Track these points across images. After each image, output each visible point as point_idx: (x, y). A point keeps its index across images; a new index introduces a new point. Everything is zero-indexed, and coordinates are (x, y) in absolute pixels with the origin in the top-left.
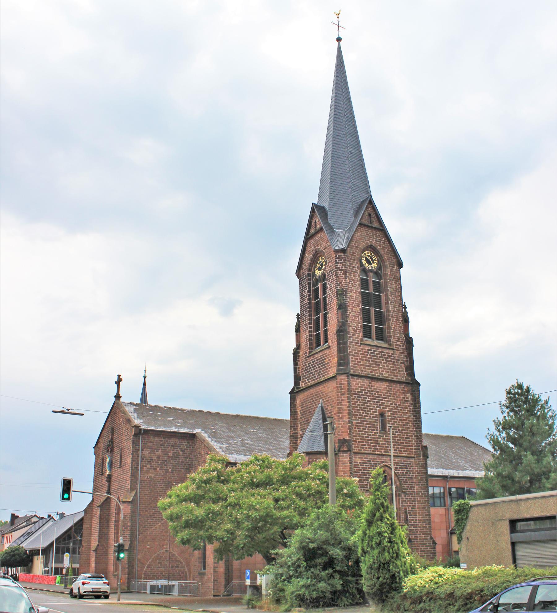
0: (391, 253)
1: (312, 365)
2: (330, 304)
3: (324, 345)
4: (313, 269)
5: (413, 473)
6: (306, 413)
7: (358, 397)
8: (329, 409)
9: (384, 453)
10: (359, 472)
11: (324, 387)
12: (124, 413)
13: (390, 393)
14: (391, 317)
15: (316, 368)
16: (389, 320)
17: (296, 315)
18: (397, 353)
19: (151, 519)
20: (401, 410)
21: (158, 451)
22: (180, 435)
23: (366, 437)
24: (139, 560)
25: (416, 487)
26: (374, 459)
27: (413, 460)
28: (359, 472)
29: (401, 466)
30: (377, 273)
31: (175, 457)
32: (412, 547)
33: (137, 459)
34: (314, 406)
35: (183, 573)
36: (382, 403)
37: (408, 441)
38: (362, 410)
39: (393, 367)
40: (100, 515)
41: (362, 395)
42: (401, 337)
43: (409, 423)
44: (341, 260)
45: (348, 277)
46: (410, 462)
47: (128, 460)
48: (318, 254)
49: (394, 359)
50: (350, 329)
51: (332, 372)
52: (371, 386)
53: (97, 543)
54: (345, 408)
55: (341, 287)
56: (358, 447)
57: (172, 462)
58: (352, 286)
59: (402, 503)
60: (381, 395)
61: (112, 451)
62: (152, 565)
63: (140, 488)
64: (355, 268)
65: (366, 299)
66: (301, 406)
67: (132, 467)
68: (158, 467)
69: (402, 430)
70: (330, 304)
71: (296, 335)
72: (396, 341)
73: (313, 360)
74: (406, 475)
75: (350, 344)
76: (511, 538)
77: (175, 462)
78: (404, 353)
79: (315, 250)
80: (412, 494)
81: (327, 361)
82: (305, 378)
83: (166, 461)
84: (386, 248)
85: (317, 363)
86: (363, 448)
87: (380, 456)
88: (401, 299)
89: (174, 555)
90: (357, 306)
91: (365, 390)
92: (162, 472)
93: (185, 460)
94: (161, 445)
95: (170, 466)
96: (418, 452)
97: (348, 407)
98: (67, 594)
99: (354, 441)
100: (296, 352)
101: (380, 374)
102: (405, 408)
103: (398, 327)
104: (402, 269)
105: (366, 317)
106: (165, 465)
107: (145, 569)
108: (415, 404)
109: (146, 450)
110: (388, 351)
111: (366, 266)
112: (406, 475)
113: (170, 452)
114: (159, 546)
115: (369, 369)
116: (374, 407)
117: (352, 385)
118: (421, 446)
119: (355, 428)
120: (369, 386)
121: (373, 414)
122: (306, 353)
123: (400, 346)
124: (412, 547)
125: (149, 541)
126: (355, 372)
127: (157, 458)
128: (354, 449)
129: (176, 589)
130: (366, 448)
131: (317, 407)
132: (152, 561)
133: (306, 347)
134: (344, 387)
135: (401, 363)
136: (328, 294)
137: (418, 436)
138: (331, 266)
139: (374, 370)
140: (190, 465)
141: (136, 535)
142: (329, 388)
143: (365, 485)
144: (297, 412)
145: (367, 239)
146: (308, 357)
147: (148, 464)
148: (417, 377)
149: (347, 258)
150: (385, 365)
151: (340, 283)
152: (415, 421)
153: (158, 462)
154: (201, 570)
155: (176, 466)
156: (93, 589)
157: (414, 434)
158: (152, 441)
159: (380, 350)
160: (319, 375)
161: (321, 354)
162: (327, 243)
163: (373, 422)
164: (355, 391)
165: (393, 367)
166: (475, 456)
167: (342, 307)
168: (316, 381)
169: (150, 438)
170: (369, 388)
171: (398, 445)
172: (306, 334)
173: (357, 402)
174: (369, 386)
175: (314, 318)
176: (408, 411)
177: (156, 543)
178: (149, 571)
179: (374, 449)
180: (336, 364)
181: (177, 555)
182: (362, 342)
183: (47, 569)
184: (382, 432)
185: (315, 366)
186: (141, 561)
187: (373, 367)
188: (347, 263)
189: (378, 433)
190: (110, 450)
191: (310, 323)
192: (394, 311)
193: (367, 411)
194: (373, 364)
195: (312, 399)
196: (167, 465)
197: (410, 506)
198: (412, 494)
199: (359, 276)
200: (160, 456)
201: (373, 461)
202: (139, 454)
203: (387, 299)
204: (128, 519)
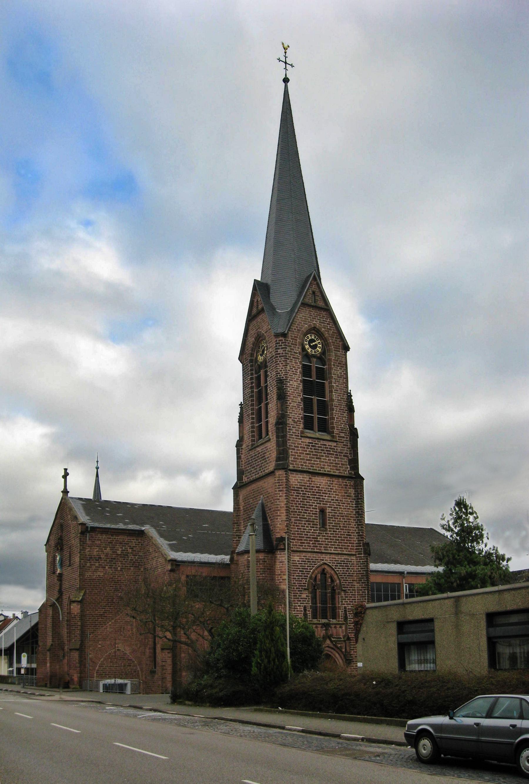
0: (337, 336)
1: (254, 459)
2: (271, 394)
3: (266, 437)
4: (255, 354)
5: (353, 571)
6: (249, 510)
7: (296, 493)
8: (269, 505)
9: (323, 551)
10: (297, 571)
11: (265, 482)
12: (71, 509)
13: (331, 489)
14: (335, 406)
15: (258, 462)
16: (333, 410)
19: (101, 619)
20: (343, 506)
21: (106, 549)
22: (127, 532)
23: (305, 535)
24: (91, 659)
25: (357, 585)
26: (313, 557)
27: (354, 558)
28: (297, 571)
29: (341, 564)
30: (321, 359)
31: (123, 555)
32: (351, 645)
34: (255, 502)
35: (136, 672)
36: (322, 499)
37: (350, 538)
38: (301, 507)
39: (335, 461)
41: (302, 491)
42: (345, 428)
43: (351, 520)
44: (282, 346)
45: (289, 364)
46: (351, 559)
47: (77, 559)
48: (260, 337)
49: (337, 452)
50: (290, 421)
51: (271, 467)
52: (312, 481)
55: (281, 375)
56: (296, 545)
58: (293, 374)
59: (342, 602)
60: (322, 490)
61: (62, 549)
64: (297, 353)
66: (244, 502)
67: (80, 566)
68: (107, 565)
69: (343, 527)
70: (271, 394)
71: (239, 425)
72: (339, 432)
73: (255, 453)
74: (346, 573)
75: (289, 437)
76: (488, 632)
77: (124, 559)
78: (347, 445)
79: (257, 333)
80: (353, 592)
81: (267, 455)
82: (248, 473)
83: (115, 559)
84: (331, 330)
85: (259, 456)
86: (302, 546)
87: (320, 554)
88: (347, 387)
89: (126, 654)
90: (298, 395)
91: (305, 486)
92: (111, 570)
94: (109, 543)
95: (119, 564)
96: (359, 549)
97: (286, 504)
99: (293, 539)
100: (239, 445)
101: (321, 468)
102: (347, 504)
103: (343, 417)
104: (348, 353)
105: (307, 405)
106: (113, 563)
108: (358, 499)
110: (330, 443)
111: (309, 351)
112: (346, 573)
113: (118, 550)
115: (309, 463)
116: (314, 503)
117: (291, 481)
118: (363, 543)
119: (294, 526)
120: (309, 481)
121: (313, 511)
122: (249, 446)
123: (344, 437)
124: (351, 645)
126: (295, 467)
128: (292, 548)
129: (129, 687)
130: (305, 546)
131: (258, 503)
132: (104, 660)
133: (248, 439)
135: (344, 456)
136: (268, 382)
137: (359, 533)
138: (271, 352)
139: (314, 464)
141: (87, 634)
142: (268, 483)
143: (304, 583)
144: (240, 508)
145: (311, 320)
146: (250, 450)
147: (96, 563)
148: (362, 472)
149: (288, 343)
150: (327, 458)
152: (357, 517)
153: (107, 561)
157: (356, 530)
158: (100, 539)
159: (322, 442)
160: (260, 470)
161: (262, 447)
162: (268, 326)
163: (313, 519)
164: (294, 487)
165: (335, 461)
167: (282, 396)
169: (97, 535)
170: (310, 484)
171: (339, 543)
172: (248, 425)
173: (296, 498)
174: (309, 481)
175: (257, 408)
176: (350, 506)
177: (107, 642)
179: (313, 546)
180: (275, 459)
182: (303, 435)
183: (11, 669)
184: (322, 529)
185: (257, 460)
187: (314, 461)
190: (59, 548)
192: (338, 400)
193: (307, 508)
194: (314, 458)
195: (254, 495)
197: (350, 604)
198: (353, 592)
199: (300, 363)
200: (108, 554)
201: (311, 559)
203: (331, 387)
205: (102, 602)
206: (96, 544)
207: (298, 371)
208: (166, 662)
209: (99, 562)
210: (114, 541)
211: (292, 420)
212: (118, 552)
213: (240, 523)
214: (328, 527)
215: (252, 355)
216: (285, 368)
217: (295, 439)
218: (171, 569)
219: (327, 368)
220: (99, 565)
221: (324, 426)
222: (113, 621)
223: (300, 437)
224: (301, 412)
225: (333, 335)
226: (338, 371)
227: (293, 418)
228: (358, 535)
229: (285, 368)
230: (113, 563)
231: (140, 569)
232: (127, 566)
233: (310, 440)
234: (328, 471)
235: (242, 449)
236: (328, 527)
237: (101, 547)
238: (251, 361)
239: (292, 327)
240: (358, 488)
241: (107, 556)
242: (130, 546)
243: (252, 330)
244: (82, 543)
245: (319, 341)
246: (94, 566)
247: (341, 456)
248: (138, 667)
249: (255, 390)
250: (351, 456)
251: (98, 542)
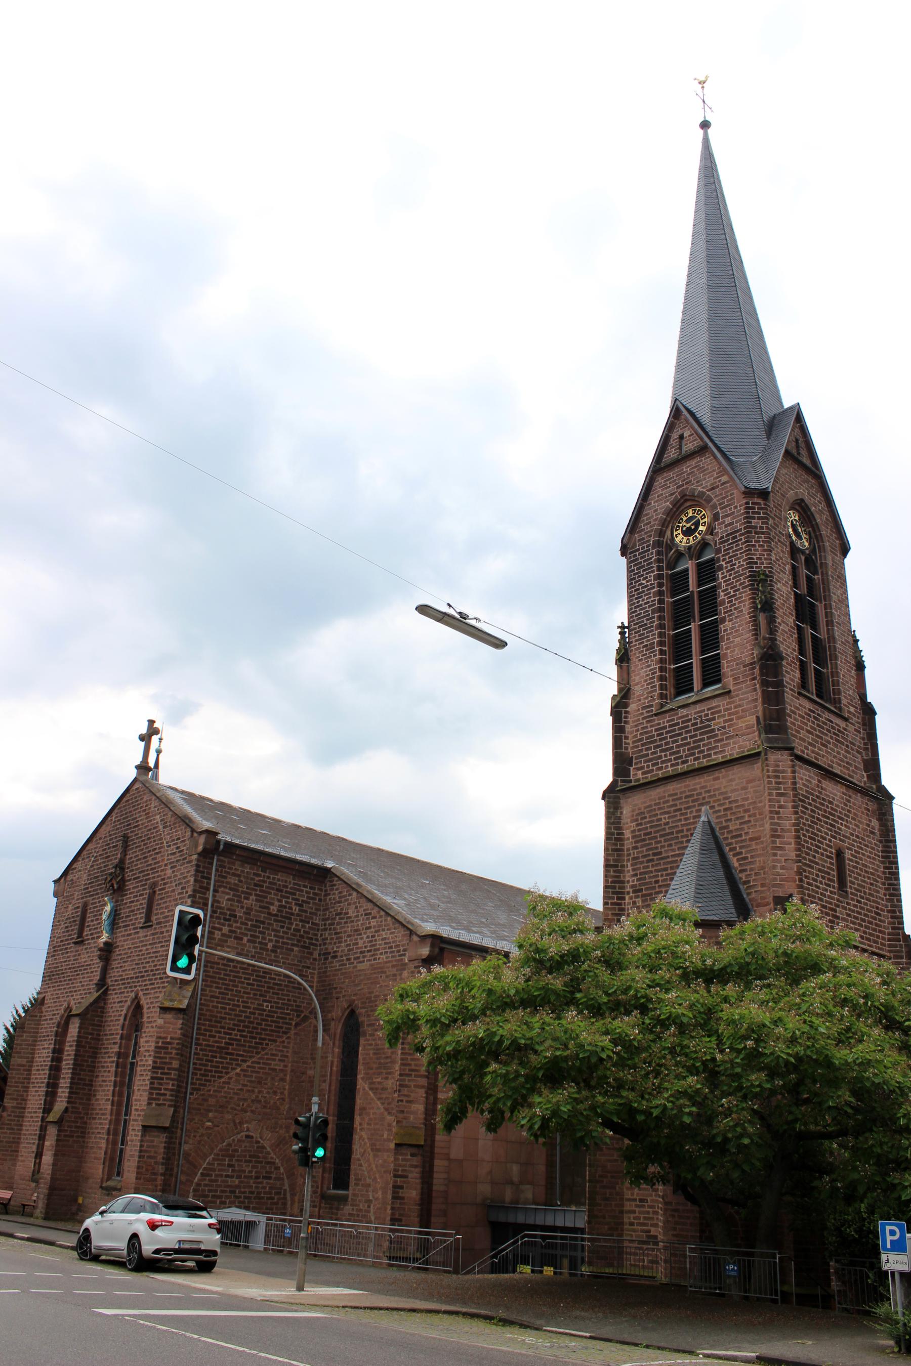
3: (702, 690)
17: (619, 627)
18: (851, 728)
19: (221, 1058)
21: (247, 899)
24: (187, 1155)
31: (282, 916)
35: (279, 1193)
40: (79, 1037)
53: (65, 1105)
54: (787, 824)
57: (275, 927)
62: (214, 1170)
63: (203, 980)
68: (246, 935)
77: (282, 927)
89: (264, 1147)
92: (254, 947)
93: (303, 926)
94: (256, 885)
95: (270, 935)
96: (896, 946)
97: (794, 825)
98: (72, 1248)
100: (619, 709)
106: (260, 932)
107: (196, 1180)
109: (223, 892)
113: (273, 904)
114: (232, 1124)
125: (211, 1111)
127: (245, 913)
129: (261, 1230)
134: (783, 777)
140: (311, 939)
141: (186, 1093)
144: (623, 834)
146: (656, 715)
147: (224, 925)
151: (758, 559)
153: (247, 924)
154: (329, 1189)
155: (283, 937)
156: (180, 1241)
158: (239, 872)
168: (680, 768)
175: (672, 633)
178: (206, 1185)
181: (269, 1149)
186: (190, 1158)
188: (771, 522)
191: (661, 643)
196: (264, 933)
200: (251, 910)
202: (207, 899)
204: (174, 1052)
205: (225, 1018)
206: (228, 883)
208: (406, 1177)
209: (230, 926)
210: (265, 882)
212: (272, 907)
213: (623, 866)
215: (661, 533)
216: (768, 555)
218: (429, 956)
220: (230, 931)
222: (245, 1065)
230: (260, 932)
231: (311, 954)
232: (287, 944)
235: (626, 712)
237: (238, 891)
238: (658, 544)
241: (249, 914)
242: (298, 900)
243: (664, 487)
246: (223, 932)
248: (286, 1181)
249: (666, 599)
250: (867, 755)
251: (233, 880)
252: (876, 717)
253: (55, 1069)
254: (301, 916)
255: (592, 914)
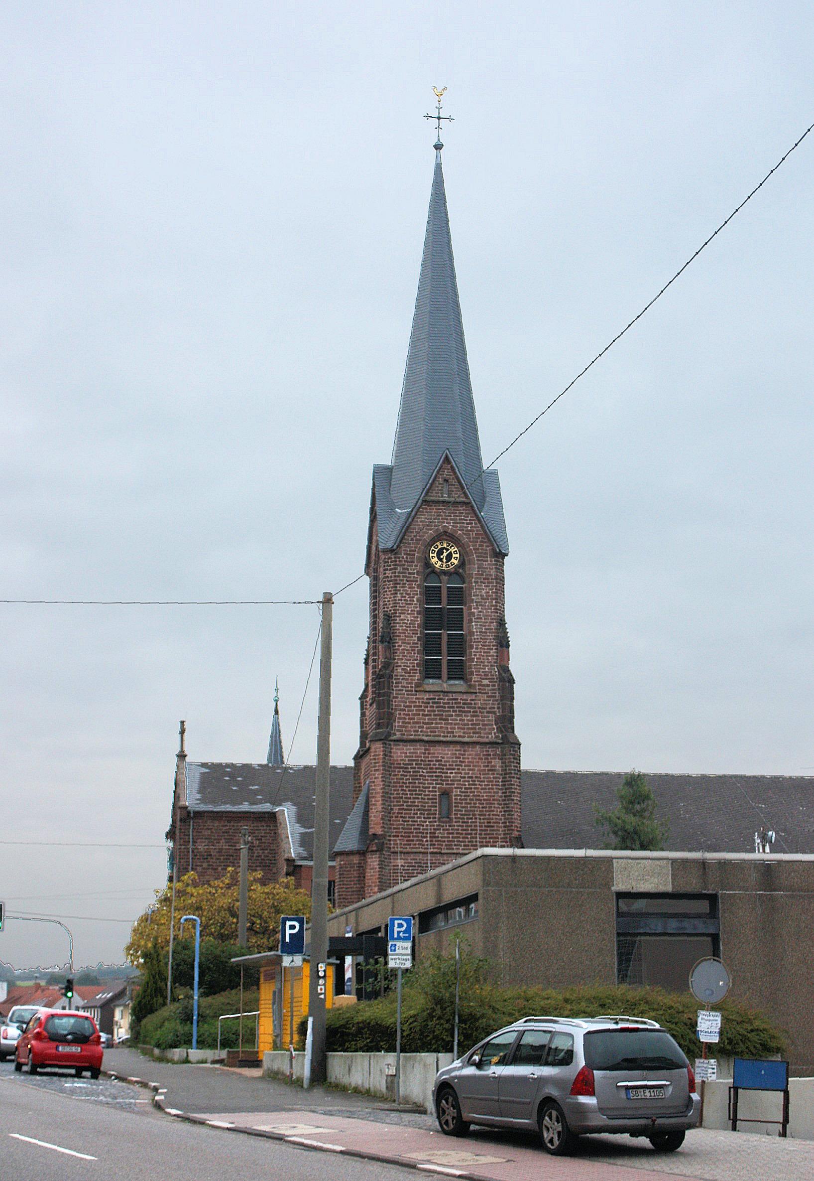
21: (219, 843)
22: (252, 815)
23: (415, 829)
30: (458, 573)
33: (187, 855)
45: (400, 590)
64: (414, 574)
65: (431, 619)
94: (223, 833)
105: (430, 645)
110: (465, 697)
120: (424, 753)
123: (488, 686)
130: (415, 844)
137: (506, 823)
149: (400, 561)
158: (211, 827)
166: (207, 896)
169: (206, 822)
174: (424, 753)
182: (417, 689)
188: (399, 569)
189: (435, 822)
207: (415, 599)
211: (402, 669)
214: (453, 816)
217: (406, 696)
219: (466, 587)
221: (458, 671)
223: (414, 693)
224: (417, 657)
225: (477, 538)
226: (484, 590)
227: (404, 666)
228: (504, 827)
229: (394, 597)
231: (271, 870)
233: (431, 694)
234: (459, 736)
235: (366, 702)
236: (453, 816)
239: (406, 537)
240: (505, 759)
244: (182, 834)
245: (456, 549)
246: (204, 866)
247: (468, 716)
250: (499, 712)
252: (515, 685)
253: (637, 1022)
254: (261, 846)
255: (173, 860)
